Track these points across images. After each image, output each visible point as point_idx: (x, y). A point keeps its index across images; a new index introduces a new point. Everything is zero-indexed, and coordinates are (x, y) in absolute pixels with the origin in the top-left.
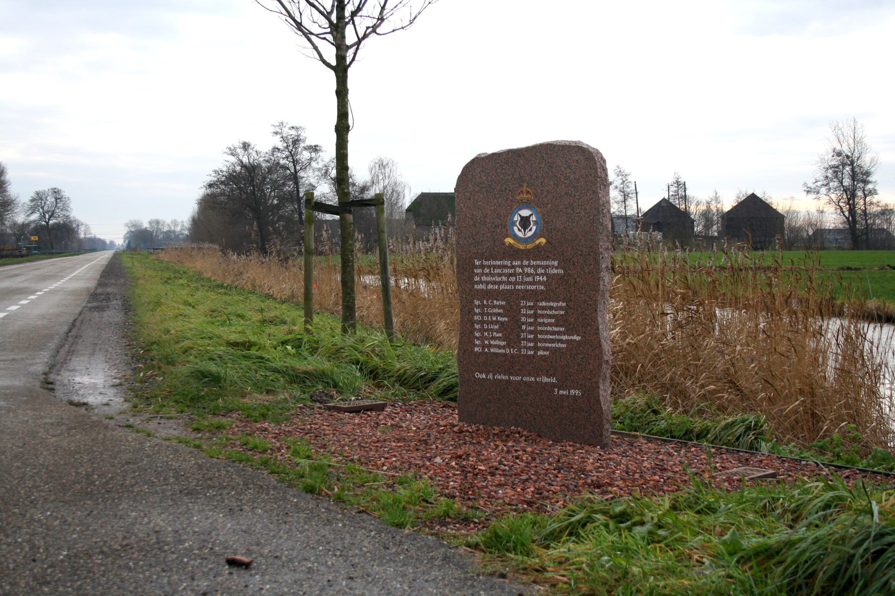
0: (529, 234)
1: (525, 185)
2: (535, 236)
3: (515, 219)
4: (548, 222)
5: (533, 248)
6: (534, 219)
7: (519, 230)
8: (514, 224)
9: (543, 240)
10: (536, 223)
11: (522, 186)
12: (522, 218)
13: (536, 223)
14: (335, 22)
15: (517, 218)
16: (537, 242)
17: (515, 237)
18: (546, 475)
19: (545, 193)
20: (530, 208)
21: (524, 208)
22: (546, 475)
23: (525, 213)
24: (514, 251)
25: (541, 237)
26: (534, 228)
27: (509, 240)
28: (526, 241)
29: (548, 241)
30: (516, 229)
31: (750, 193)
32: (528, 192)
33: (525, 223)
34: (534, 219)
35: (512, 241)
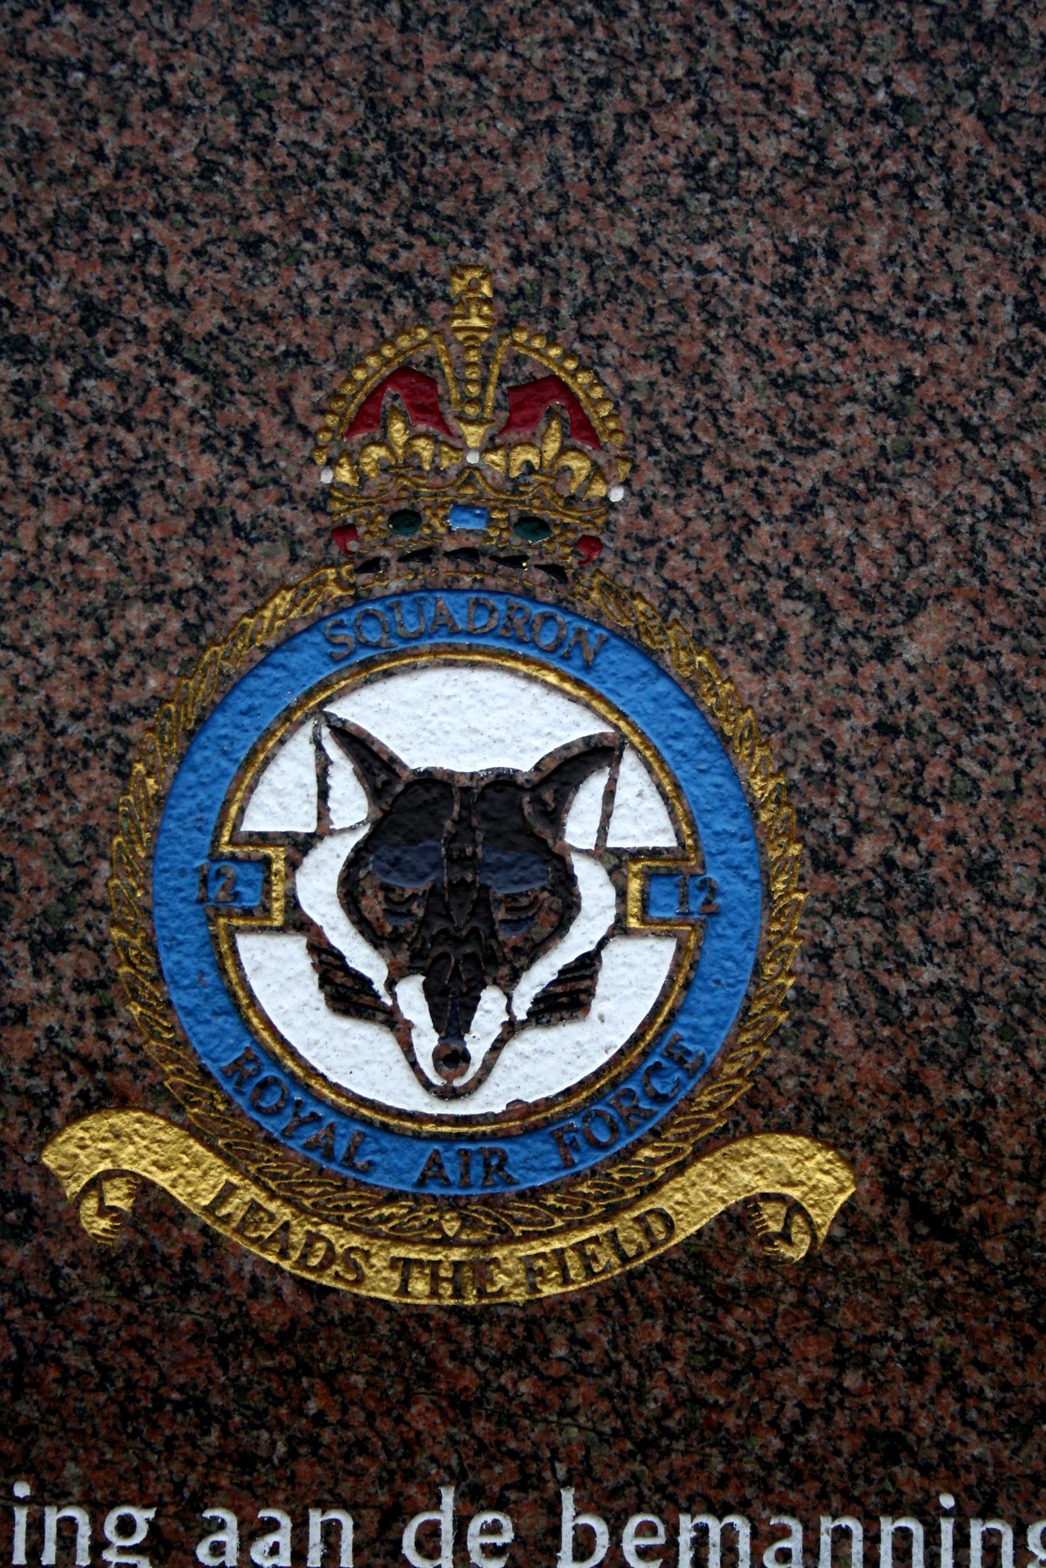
0: (548, 1064)
1: (478, 283)
2: (639, 1102)
3: (281, 798)
4: (894, 894)
5: (619, 1298)
6: (642, 819)
7: (347, 994)
8: (249, 883)
9: (808, 1178)
10: (664, 887)
11: (426, 298)
12: (409, 803)
13: (664, 887)
14: (253, 949)
15: (293, 791)
16: (697, 1199)
17: (260, 1100)
18: (361, 1446)
19: (861, 437)
20: (571, 664)
21: (452, 647)
22: (361, 1446)
23: (469, 718)
24: (226, 1341)
25: (759, 1112)
26: (636, 977)
27: (116, 1156)
28: (479, 1171)
29: (889, 1178)
30: (277, 975)
31: (597, 1006)
32: (531, 400)
33: (461, 881)
34: (642, 819)
35: (195, 1178)
